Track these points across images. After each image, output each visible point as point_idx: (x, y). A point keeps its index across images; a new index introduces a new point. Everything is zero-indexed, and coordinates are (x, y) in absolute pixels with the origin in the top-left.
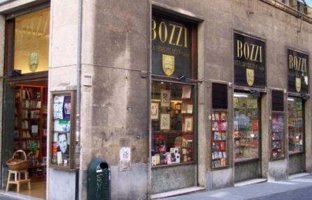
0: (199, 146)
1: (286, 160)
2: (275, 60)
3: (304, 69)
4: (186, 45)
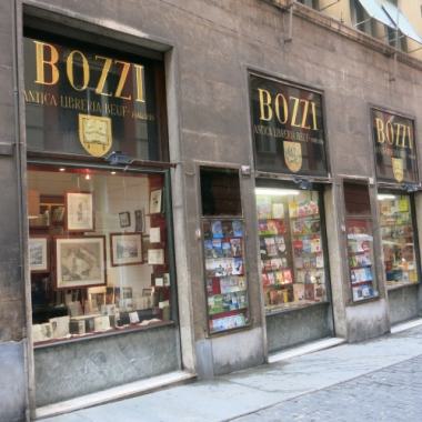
0: (180, 291)
1: (383, 301)
2: (347, 127)
3: (407, 143)
4: (315, 128)
